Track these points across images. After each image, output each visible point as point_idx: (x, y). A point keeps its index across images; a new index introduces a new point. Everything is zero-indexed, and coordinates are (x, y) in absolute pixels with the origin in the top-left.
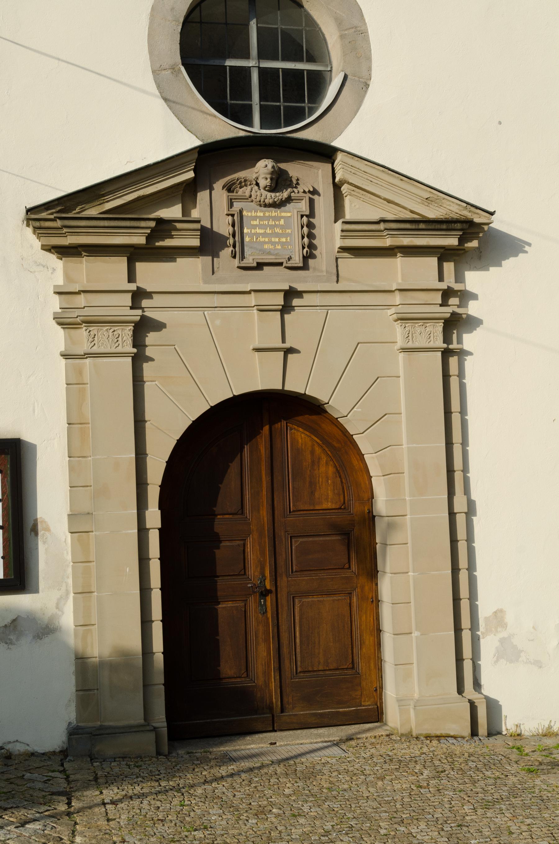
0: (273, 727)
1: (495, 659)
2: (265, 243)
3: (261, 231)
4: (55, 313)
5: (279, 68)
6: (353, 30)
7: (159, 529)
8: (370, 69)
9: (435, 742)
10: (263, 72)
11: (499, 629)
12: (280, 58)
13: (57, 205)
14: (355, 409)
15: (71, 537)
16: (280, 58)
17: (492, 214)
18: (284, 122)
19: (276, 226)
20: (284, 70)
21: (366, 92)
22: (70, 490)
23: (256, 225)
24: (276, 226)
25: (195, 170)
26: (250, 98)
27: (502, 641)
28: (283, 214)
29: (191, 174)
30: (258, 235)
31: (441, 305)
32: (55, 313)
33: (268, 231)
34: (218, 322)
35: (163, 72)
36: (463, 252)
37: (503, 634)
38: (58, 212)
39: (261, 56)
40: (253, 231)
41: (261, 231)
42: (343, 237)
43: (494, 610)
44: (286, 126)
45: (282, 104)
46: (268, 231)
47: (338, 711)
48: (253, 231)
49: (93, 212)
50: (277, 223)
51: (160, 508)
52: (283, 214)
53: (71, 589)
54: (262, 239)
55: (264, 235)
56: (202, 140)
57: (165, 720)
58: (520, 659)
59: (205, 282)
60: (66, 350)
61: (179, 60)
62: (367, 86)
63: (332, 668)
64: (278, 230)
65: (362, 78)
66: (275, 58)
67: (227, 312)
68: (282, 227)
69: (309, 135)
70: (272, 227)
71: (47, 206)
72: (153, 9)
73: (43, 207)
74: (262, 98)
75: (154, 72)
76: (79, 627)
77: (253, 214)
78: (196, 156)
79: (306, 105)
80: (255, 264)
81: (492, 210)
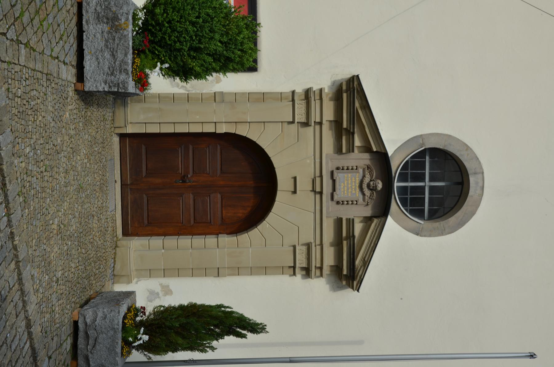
0: (124, 185)
1: (149, 290)
2: (344, 184)
3: (349, 182)
4: (312, 88)
5: (425, 195)
6: (443, 229)
7: (215, 132)
8: (425, 236)
9: (113, 257)
10: (423, 188)
11: (163, 292)
12: (430, 196)
13: (360, 89)
14: (268, 224)
15: (213, 93)
16: (430, 196)
17: (358, 291)
18: (402, 198)
19: (352, 189)
20: (424, 198)
21: (414, 234)
22: (234, 93)
23: (352, 180)
24: (352, 189)
25: (376, 152)
26: (412, 181)
27: (158, 294)
28: (357, 192)
29: (375, 150)
30: (348, 180)
31: (315, 266)
32: (312, 88)
33: (350, 186)
34: (308, 161)
35: (421, 140)
36: (340, 277)
37: (161, 295)
38: (357, 89)
39: (431, 188)
40: (349, 178)
41: (349, 182)
42: (347, 219)
43: (172, 290)
44: (399, 198)
45: (409, 196)
46: (350, 186)
47: (128, 216)
48: (349, 178)
49: (357, 104)
50: (353, 190)
51: (225, 133)
52: (357, 192)
53: (190, 92)
54: (346, 183)
55: (348, 183)
56: (391, 156)
57: (130, 132)
58: (149, 302)
59: (327, 155)
60: (296, 93)
61: (427, 147)
62: (417, 234)
63: (149, 213)
64: (350, 190)
65: (421, 232)
66: (430, 194)
67: (313, 166)
68: (351, 192)
69: (393, 206)
70: (351, 187)
71: (360, 84)
72: (450, 136)
73: (359, 82)
74: (412, 187)
75: (421, 135)
76: (50, 363)
77: (357, 178)
78: (383, 151)
79: (409, 208)
80: (334, 179)
81: (360, 291)
